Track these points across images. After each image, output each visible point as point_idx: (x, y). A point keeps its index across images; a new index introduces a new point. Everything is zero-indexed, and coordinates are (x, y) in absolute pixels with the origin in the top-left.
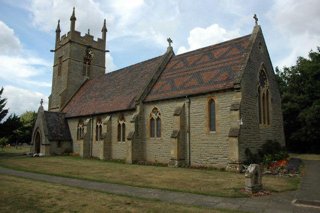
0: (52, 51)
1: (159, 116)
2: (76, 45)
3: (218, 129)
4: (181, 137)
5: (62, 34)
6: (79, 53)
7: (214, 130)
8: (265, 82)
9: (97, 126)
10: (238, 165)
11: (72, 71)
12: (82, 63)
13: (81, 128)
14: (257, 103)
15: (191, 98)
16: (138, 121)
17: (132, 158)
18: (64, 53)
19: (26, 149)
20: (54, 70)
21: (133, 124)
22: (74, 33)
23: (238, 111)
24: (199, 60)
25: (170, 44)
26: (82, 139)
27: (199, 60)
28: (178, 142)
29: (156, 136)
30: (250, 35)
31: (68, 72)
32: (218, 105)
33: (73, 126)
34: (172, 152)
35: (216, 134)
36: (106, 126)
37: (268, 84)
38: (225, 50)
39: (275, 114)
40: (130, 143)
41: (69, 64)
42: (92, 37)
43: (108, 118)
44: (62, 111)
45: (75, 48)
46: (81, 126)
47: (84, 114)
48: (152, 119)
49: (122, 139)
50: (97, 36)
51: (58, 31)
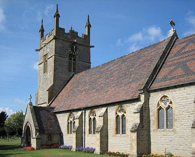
0: (93, 47)
1: (170, 105)
9: (90, 119)
11: (58, 67)
13: (71, 122)
16: (144, 112)
17: (138, 151)
18: (48, 50)
19: (17, 141)
33: (63, 120)
47: (75, 108)
49: (70, 132)
50: (82, 32)
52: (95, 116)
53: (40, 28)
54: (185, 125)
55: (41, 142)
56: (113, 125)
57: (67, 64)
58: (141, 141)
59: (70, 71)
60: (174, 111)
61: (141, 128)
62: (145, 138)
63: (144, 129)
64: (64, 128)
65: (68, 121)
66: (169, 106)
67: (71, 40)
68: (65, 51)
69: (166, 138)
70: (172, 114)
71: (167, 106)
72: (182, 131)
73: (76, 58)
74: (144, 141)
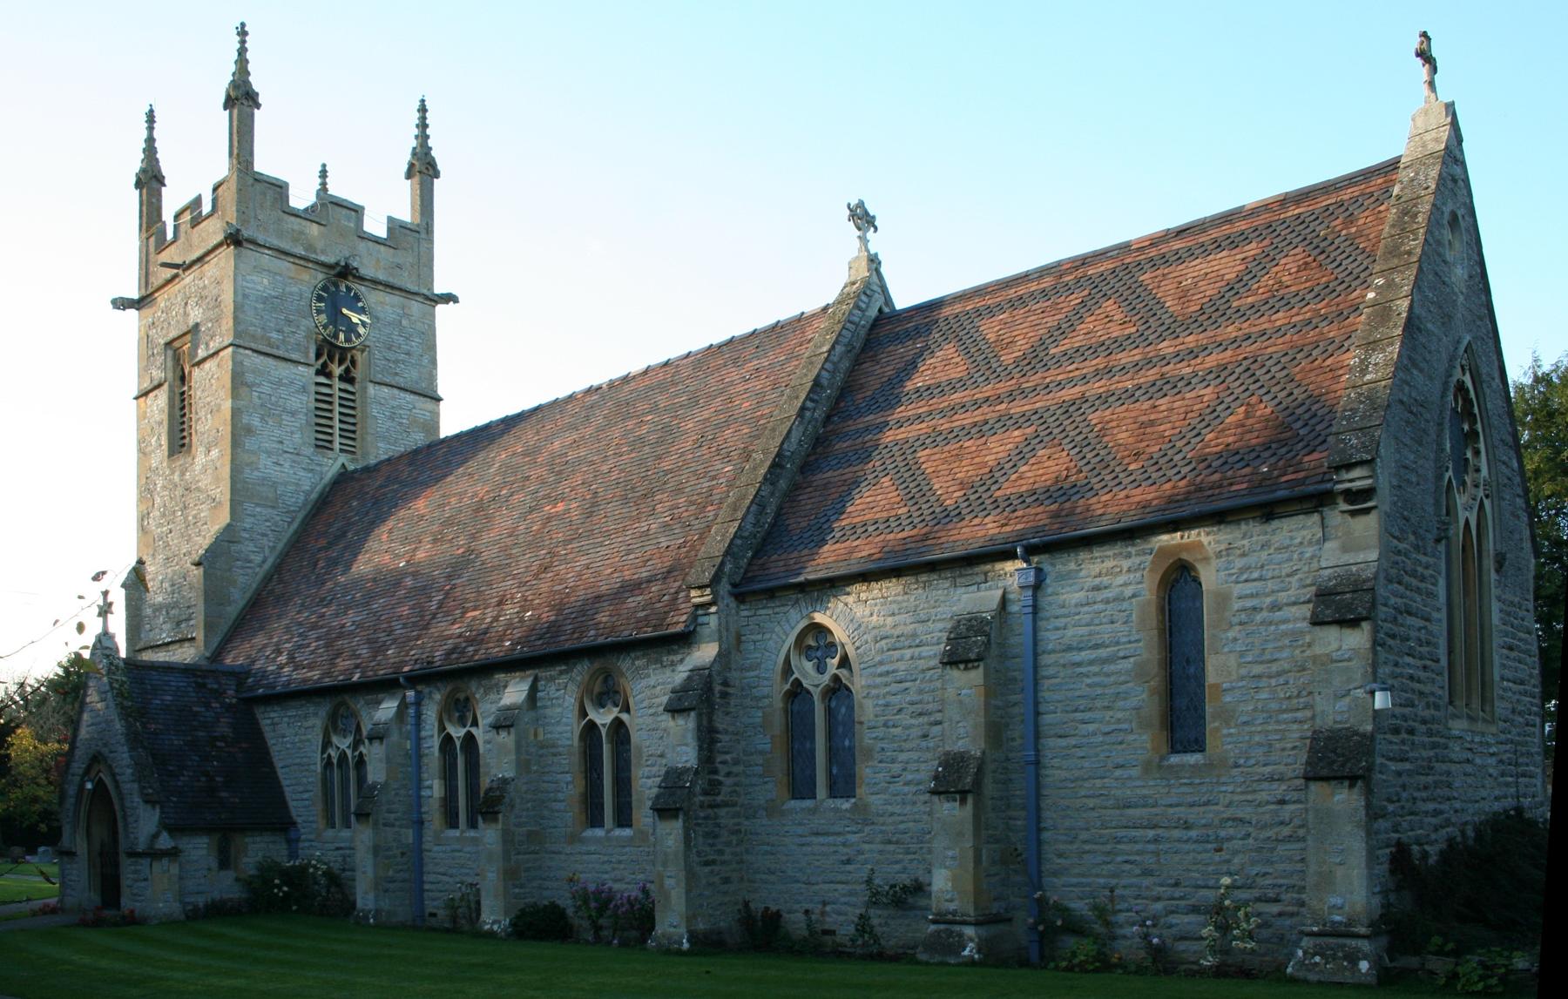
1: (843, 673)
2: (266, 259)
3: (1221, 737)
4: (989, 788)
5: (172, 200)
7: (1198, 745)
8: (1469, 455)
9: (448, 740)
10: (1365, 945)
12: (307, 374)
14: (1442, 582)
16: (702, 700)
17: (690, 918)
20: (141, 416)
21: (685, 726)
23: (1366, 626)
24: (1059, 332)
25: (863, 240)
27: (1059, 332)
28: (977, 817)
30: (1393, 165)
31: (234, 426)
32: (1223, 599)
33: (297, 743)
35: (1210, 766)
36: (506, 738)
37: (1484, 472)
38: (1227, 265)
39: (1511, 648)
40: (671, 833)
41: (238, 381)
43: (514, 692)
45: (268, 274)
46: (343, 743)
50: (384, 202)
51: (150, 180)
52: (475, 723)
53: (136, 163)
54: (910, 777)
55: (181, 878)
56: (568, 777)
58: (707, 864)
60: (861, 706)
61: (705, 793)
62: (728, 850)
63: (719, 798)
64: (306, 796)
65: (324, 751)
66: (836, 678)
67: (323, 252)
68: (290, 322)
69: (824, 849)
70: (850, 723)
71: (825, 679)
72: (897, 809)
73: (353, 362)
74: (723, 863)
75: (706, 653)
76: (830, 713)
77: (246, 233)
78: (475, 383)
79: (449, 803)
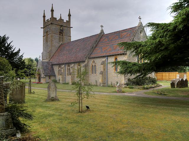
0: (41, 28)
2: (55, 25)
4: (104, 73)
5: (46, 19)
6: (56, 29)
15: (108, 57)
16: (86, 66)
20: (43, 38)
22: (53, 18)
26: (61, 75)
29: (94, 73)
30: (136, 27)
33: (56, 69)
34: (100, 80)
42: (63, 20)
43: (73, 65)
44: (49, 61)
46: (60, 69)
48: (92, 66)
50: (66, 19)
51: (44, 17)
57: (58, 38)
59: (60, 41)
75: (86, 63)
76: (95, 67)
77: (53, 23)
78: (75, 35)
79: (68, 73)
